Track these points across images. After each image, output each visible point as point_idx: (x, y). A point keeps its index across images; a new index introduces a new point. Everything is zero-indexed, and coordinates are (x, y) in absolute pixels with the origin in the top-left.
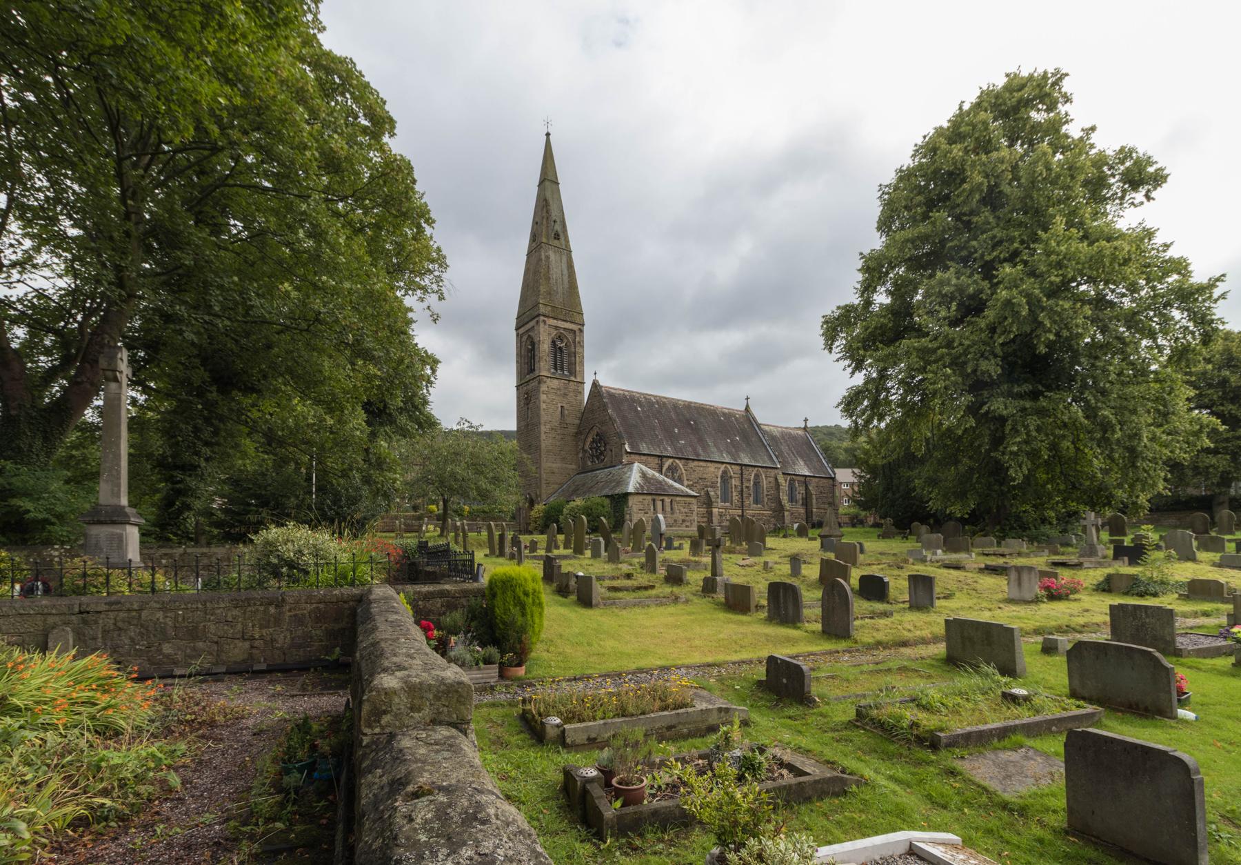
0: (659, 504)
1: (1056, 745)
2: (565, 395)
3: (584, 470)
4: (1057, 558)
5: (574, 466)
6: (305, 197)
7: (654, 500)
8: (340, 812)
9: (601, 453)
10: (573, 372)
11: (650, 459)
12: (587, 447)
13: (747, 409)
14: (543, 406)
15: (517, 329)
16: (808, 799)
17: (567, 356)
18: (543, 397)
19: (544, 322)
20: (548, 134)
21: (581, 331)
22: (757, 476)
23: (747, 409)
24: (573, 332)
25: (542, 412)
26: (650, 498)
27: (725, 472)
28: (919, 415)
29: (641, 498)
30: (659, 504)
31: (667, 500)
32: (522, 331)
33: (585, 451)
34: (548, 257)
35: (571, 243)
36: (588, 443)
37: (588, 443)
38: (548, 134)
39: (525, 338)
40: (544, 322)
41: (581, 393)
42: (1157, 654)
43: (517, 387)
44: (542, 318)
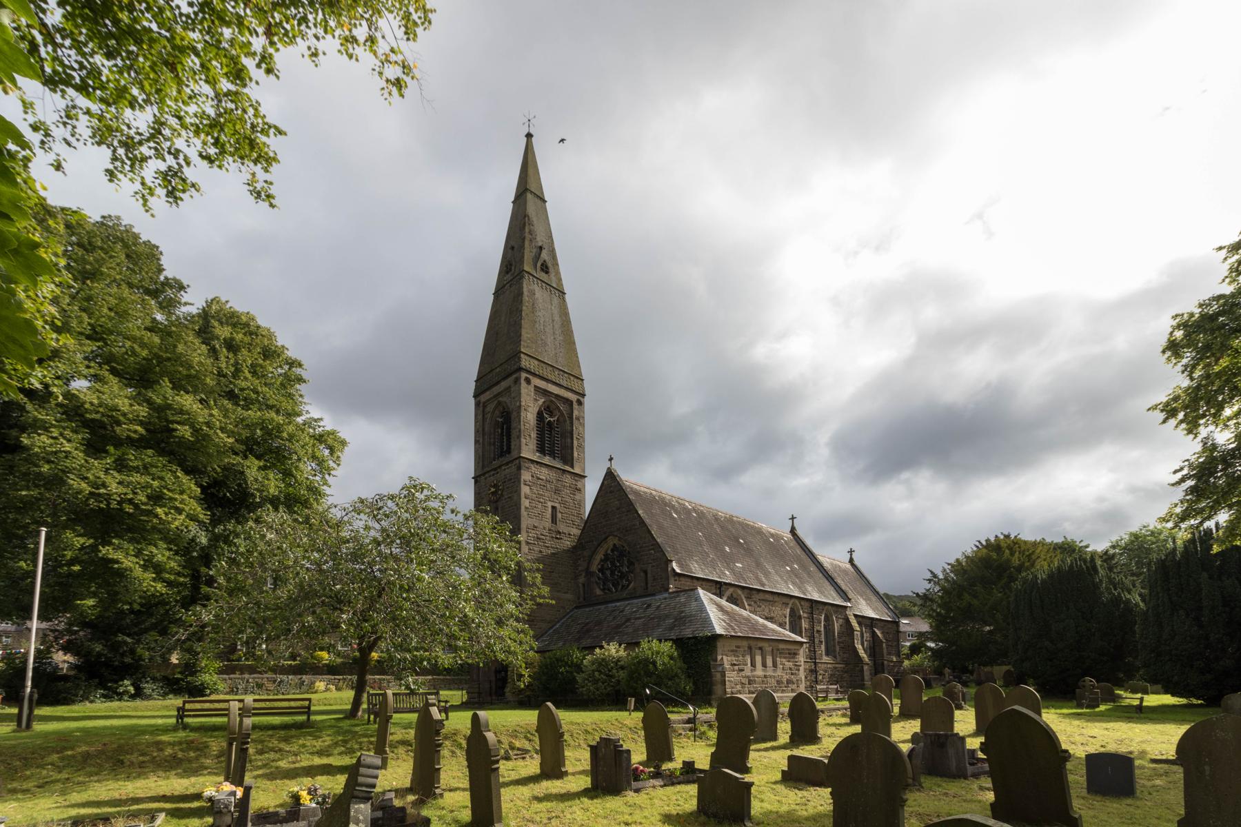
3: (586, 601)
4: (257, 697)
5: (569, 596)
8: (164, 738)
9: (623, 576)
10: (568, 459)
14: (525, 503)
15: (475, 397)
17: (559, 435)
18: (525, 490)
19: (528, 381)
20: (529, 136)
21: (580, 403)
25: (524, 513)
26: (745, 643)
28: (449, 645)
31: (768, 648)
32: (483, 398)
33: (589, 573)
34: (533, 293)
35: (564, 282)
38: (529, 136)
39: (490, 408)
40: (528, 381)
42: (30, 674)
43: (476, 479)
44: (524, 375)
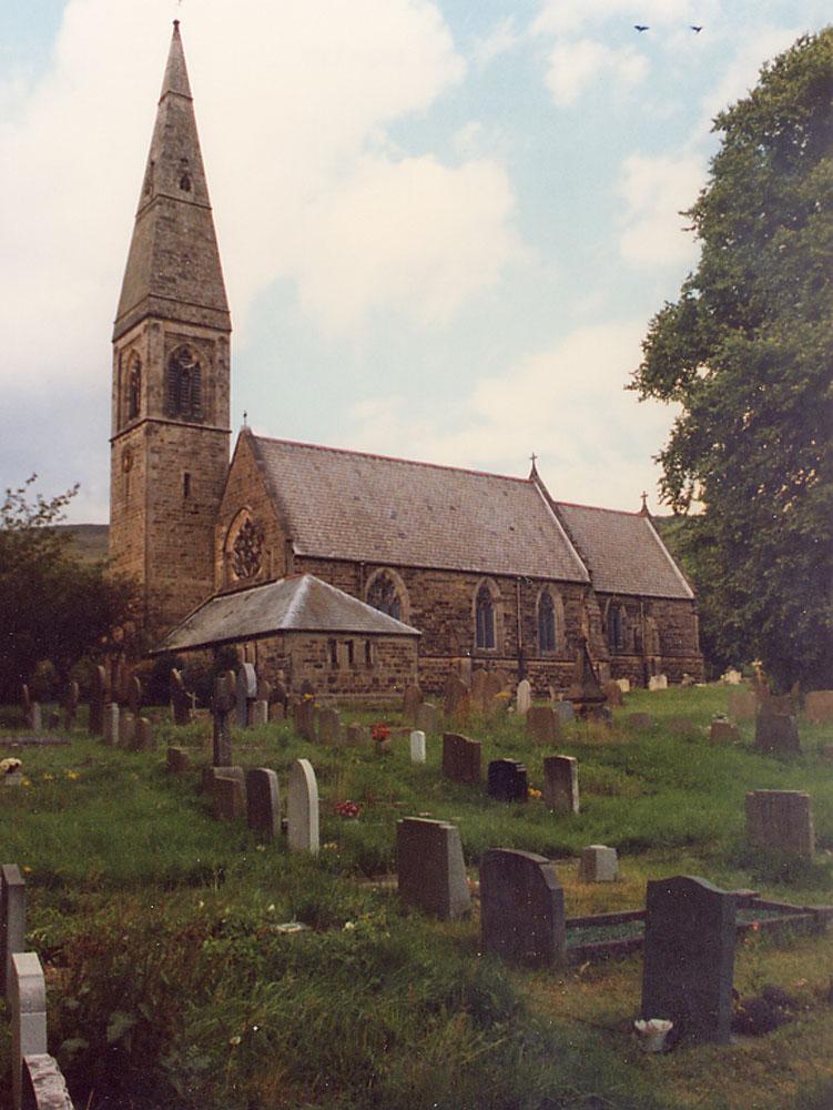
0: (342, 650)
1: (598, 878)
2: (195, 453)
6: (818, 653)
7: (333, 643)
11: (339, 569)
12: (231, 548)
13: (534, 473)
15: (114, 341)
16: (11, 1071)
21: (225, 342)
22: (544, 596)
23: (534, 473)
24: (209, 342)
26: (325, 638)
27: (484, 591)
29: (307, 639)
30: (342, 650)
31: (359, 643)
36: (232, 541)
37: (232, 541)
39: (127, 354)
41: (224, 450)
